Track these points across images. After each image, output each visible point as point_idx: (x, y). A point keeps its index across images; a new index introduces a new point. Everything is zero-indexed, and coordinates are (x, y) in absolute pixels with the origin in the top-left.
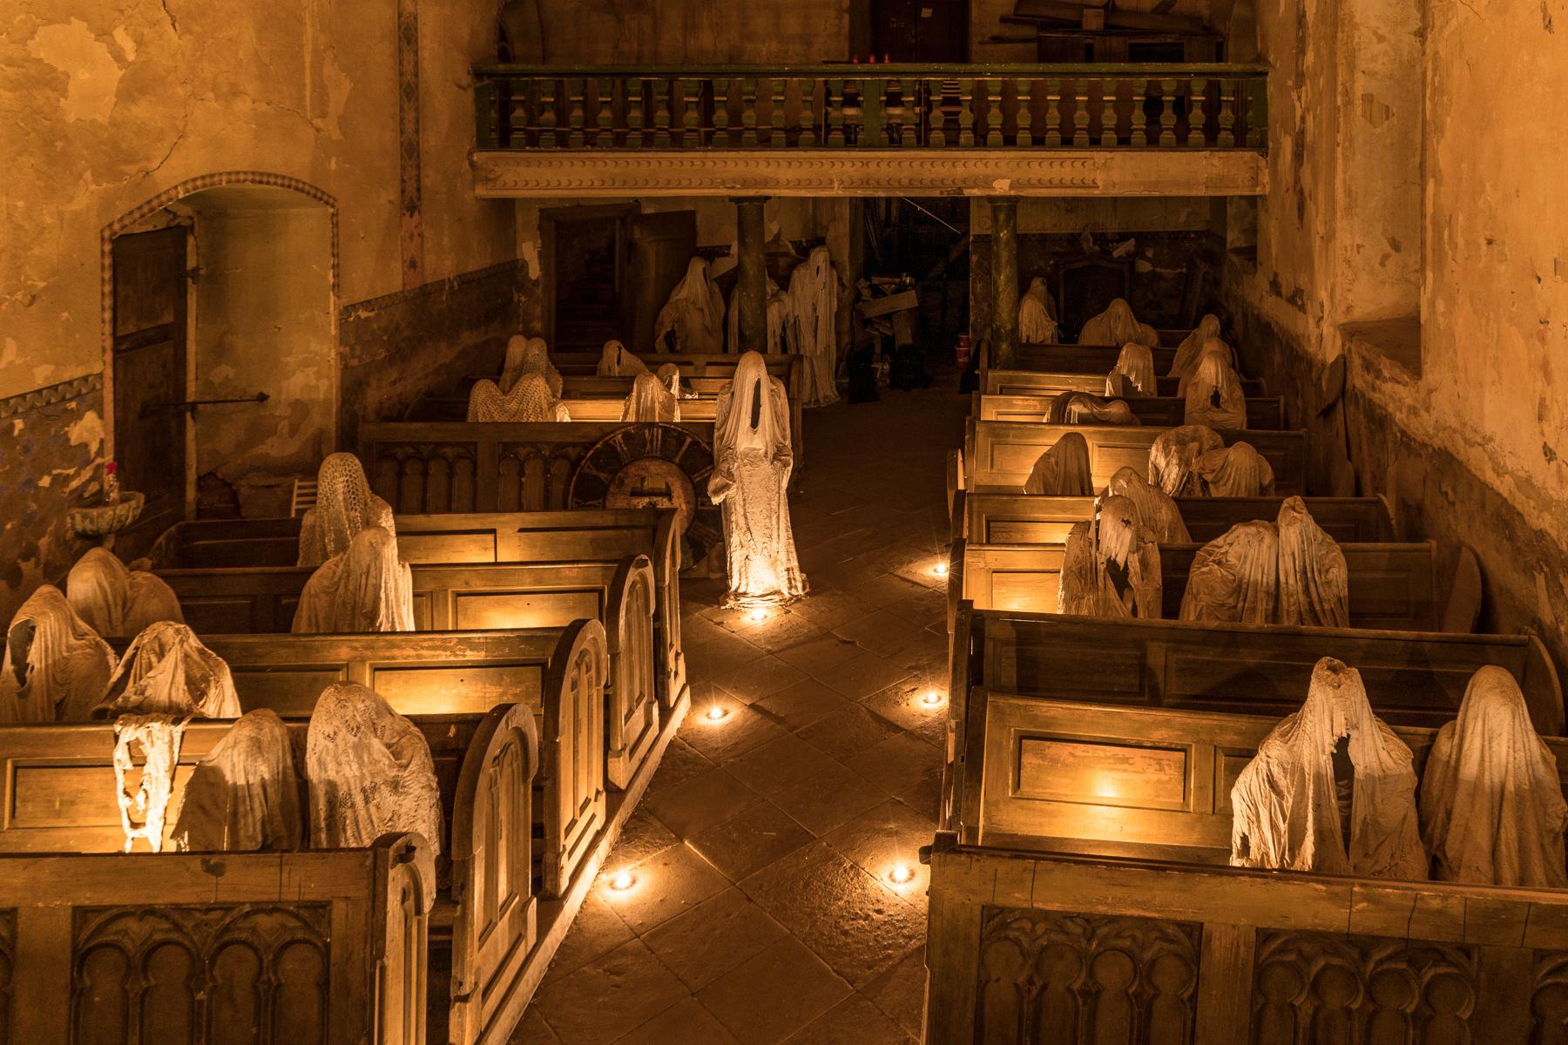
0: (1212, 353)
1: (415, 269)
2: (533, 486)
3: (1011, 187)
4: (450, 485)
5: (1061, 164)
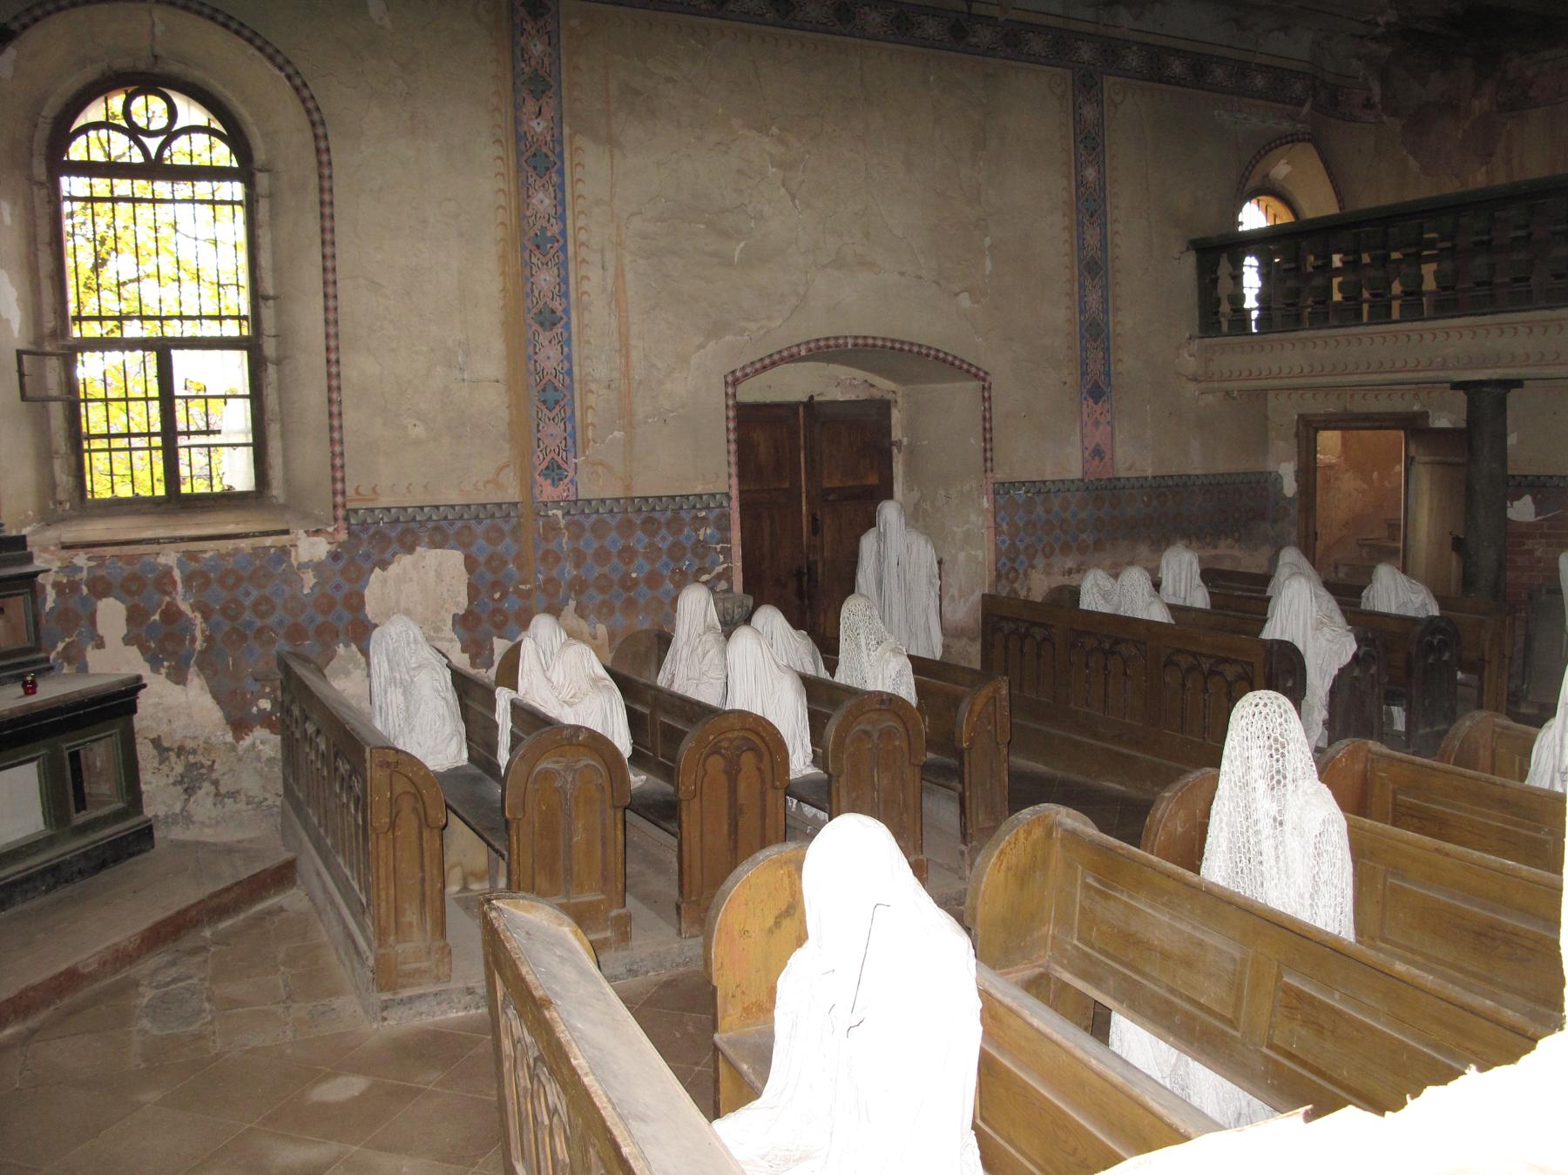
1: (1102, 459)
4: (190, 460)
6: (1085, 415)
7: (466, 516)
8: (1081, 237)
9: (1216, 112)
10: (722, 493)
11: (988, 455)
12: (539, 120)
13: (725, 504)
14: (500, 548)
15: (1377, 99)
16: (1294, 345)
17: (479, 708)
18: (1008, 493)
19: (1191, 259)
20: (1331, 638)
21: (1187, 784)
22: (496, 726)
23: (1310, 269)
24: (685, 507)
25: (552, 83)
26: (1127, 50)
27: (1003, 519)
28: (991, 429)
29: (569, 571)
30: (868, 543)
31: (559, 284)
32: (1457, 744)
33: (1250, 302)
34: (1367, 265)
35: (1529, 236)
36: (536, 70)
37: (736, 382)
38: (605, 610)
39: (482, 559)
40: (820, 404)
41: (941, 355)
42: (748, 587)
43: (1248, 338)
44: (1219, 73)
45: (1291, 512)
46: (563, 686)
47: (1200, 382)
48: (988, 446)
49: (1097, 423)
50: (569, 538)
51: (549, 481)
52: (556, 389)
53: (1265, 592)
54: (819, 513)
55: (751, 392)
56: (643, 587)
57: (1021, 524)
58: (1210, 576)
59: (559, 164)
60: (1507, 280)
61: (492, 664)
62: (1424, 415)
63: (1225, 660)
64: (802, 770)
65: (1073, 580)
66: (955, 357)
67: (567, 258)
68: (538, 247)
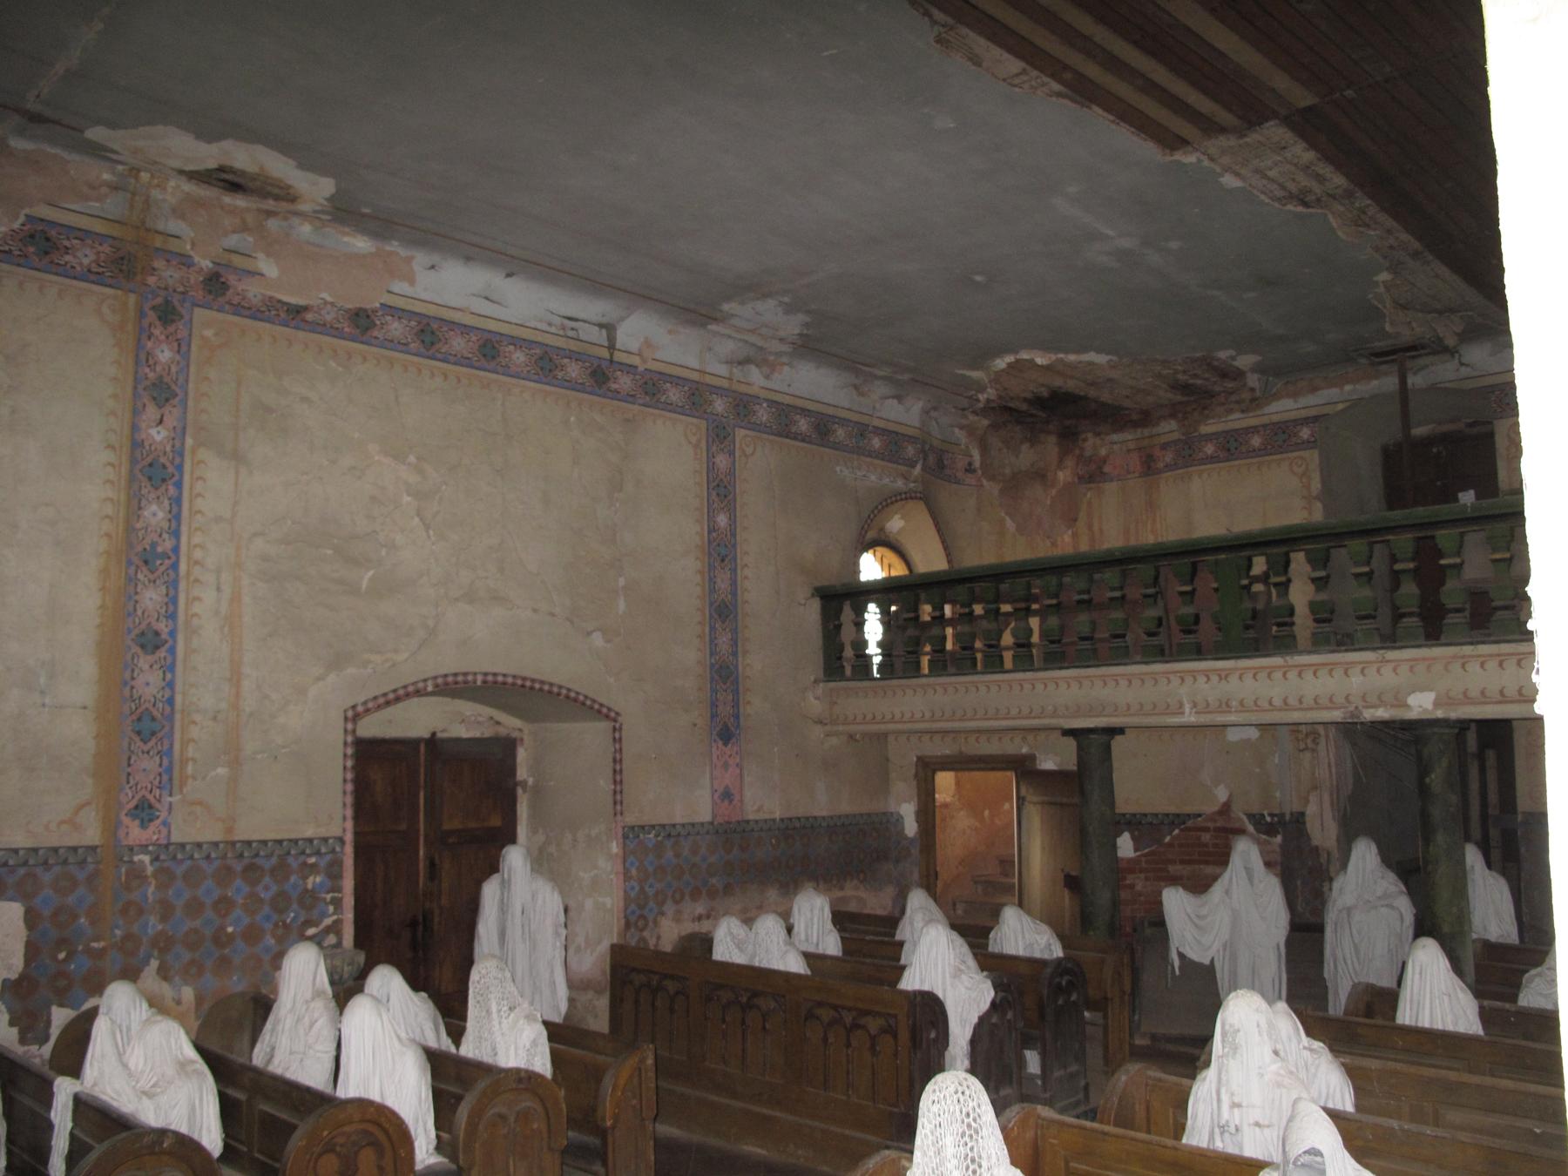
1: (731, 801)
3: (1437, 704)
6: (715, 757)
7: (31, 862)
8: (712, 580)
9: (838, 469)
10: (335, 838)
11: (618, 797)
12: (160, 428)
13: (338, 849)
14: (71, 900)
15: (977, 464)
16: (915, 691)
17: (27, 1101)
18: (638, 836)
19: (816, 605)
20: (969, 986)
21: (867, 1172)
22: (51, 1126)
23: (927, 618)
24: (293, 852)
25: (178, 391)
26: (758, 407)
27: (632, 864)
28: (621, 771)
29: (154, 924)
30: (490, 891)
31: (166, 604)
32: (1116, 1100)
33: (873, 649)
34: (980, 617)
35: (1123, 597)
36: (161, 377)
37: (356, 717)
38: (194, 970)
39: (47, 913)
40: (443, 740)
41: (573, 695)
42: (359, 942)
43: (866, 684)
45: (913, 851)
46: (143, 1072)
47: (826, 724)
48: (618, 788)
49: (726, 766)
50: (156, 888)
51: (137, 822)
52: (153, 719)
53: (893, 935)
54: (437, 857)
55: (371, 728)
56: (240, 944)
57: (651, 869)
58: (841, 919)
59: (177, 478)
60: (1107, 635)
61: (47, 1039)
62: (1032, 758)
63: (867, 1013)
64: (424, 1160)
65: (704, 927)
66: (586, 697)
67: (178, 575)
68: (146, 562)
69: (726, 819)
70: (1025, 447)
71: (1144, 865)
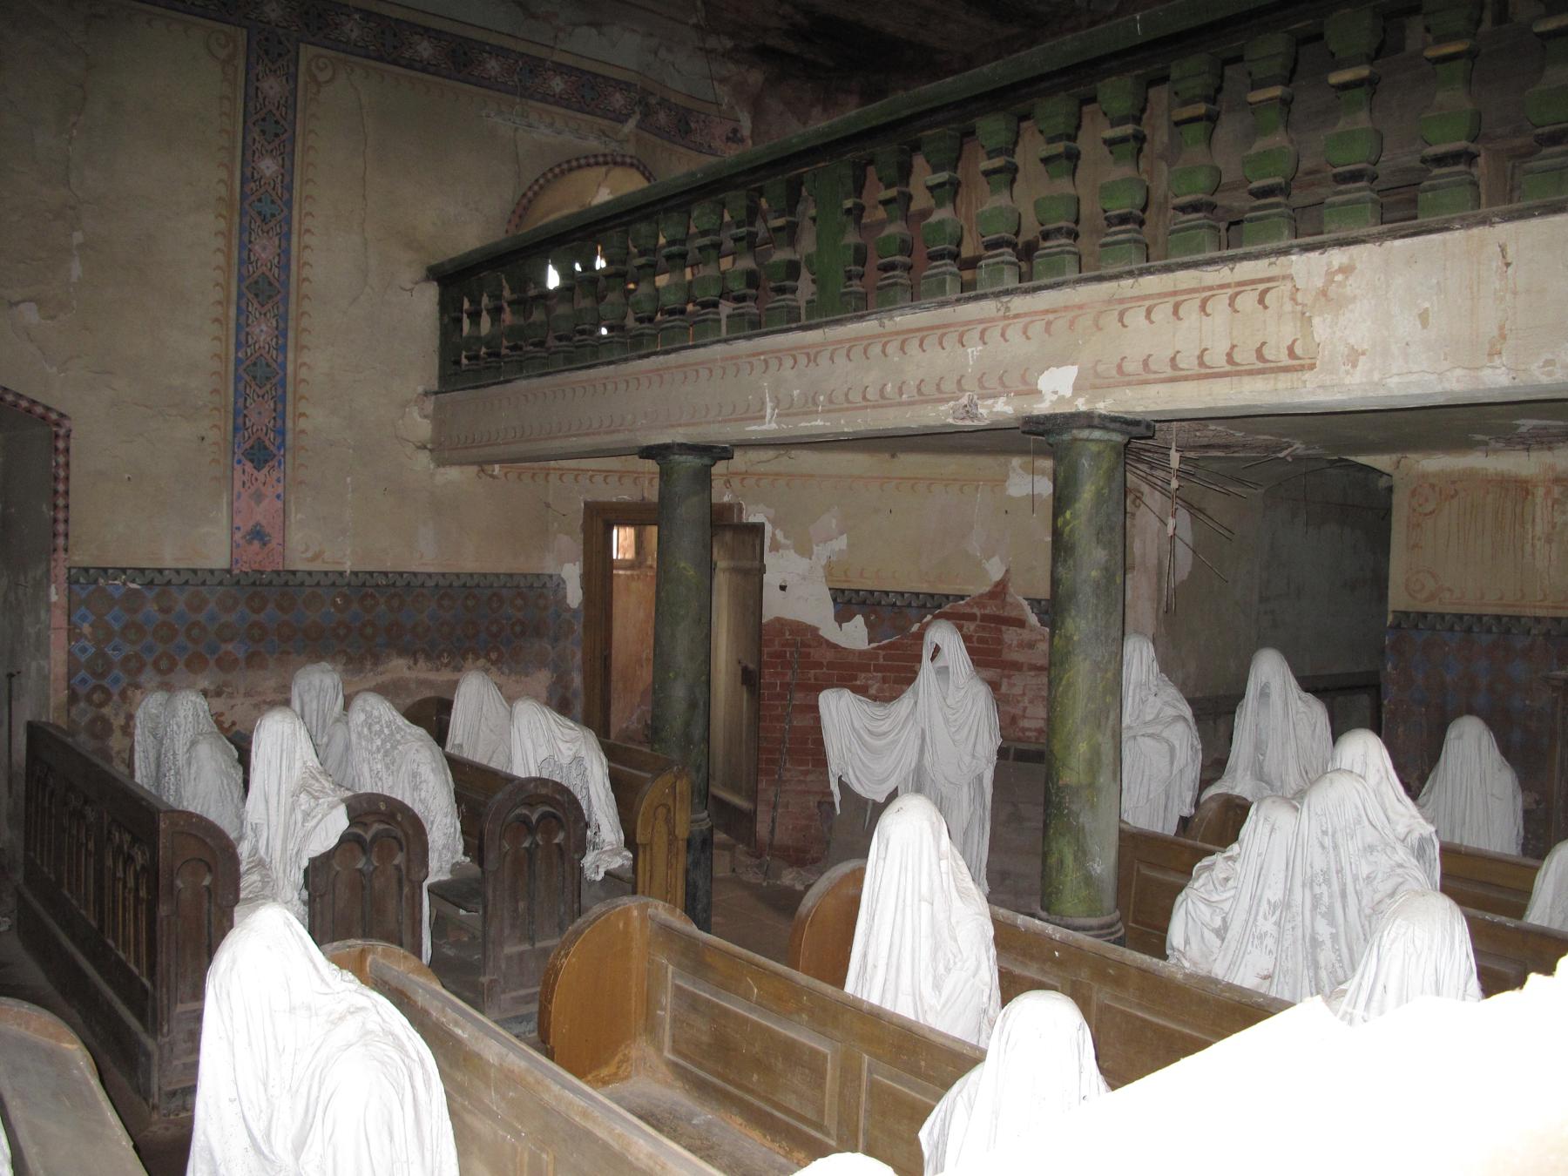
0: (724, 570)
2: (445, 717)
3: (1078, 388)
5: (1203, 308)
6: (238, 484)
18: (96, 582)
19: (432, 292)
25: (286, 126)
27: (84, 618)
44: (493, 66)
49: (259, 497)
57: (116, 627)
59: (286, 211)
69: (256, 567)
70: (816, 111)
71: (881, 661)
